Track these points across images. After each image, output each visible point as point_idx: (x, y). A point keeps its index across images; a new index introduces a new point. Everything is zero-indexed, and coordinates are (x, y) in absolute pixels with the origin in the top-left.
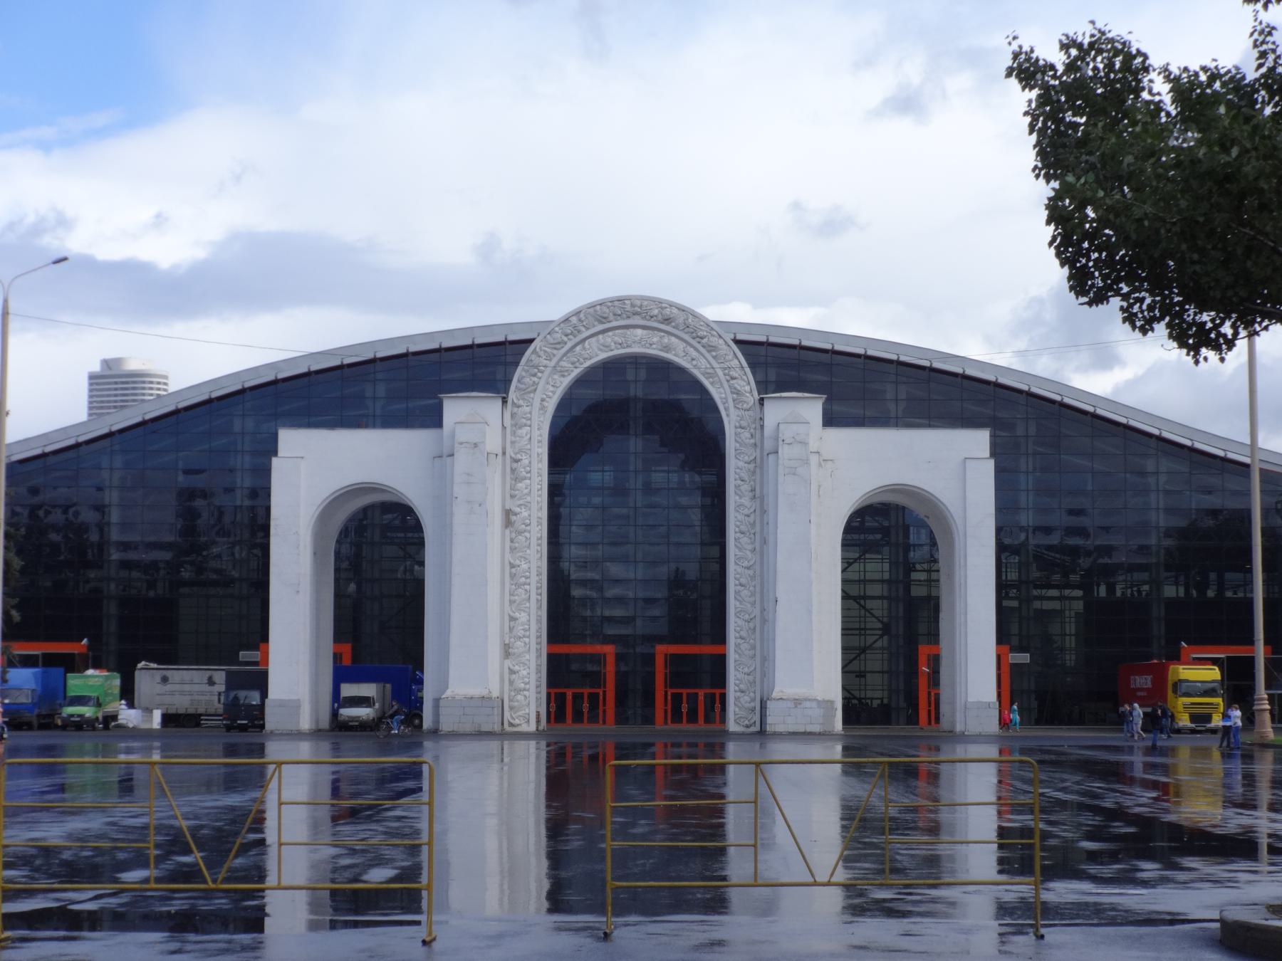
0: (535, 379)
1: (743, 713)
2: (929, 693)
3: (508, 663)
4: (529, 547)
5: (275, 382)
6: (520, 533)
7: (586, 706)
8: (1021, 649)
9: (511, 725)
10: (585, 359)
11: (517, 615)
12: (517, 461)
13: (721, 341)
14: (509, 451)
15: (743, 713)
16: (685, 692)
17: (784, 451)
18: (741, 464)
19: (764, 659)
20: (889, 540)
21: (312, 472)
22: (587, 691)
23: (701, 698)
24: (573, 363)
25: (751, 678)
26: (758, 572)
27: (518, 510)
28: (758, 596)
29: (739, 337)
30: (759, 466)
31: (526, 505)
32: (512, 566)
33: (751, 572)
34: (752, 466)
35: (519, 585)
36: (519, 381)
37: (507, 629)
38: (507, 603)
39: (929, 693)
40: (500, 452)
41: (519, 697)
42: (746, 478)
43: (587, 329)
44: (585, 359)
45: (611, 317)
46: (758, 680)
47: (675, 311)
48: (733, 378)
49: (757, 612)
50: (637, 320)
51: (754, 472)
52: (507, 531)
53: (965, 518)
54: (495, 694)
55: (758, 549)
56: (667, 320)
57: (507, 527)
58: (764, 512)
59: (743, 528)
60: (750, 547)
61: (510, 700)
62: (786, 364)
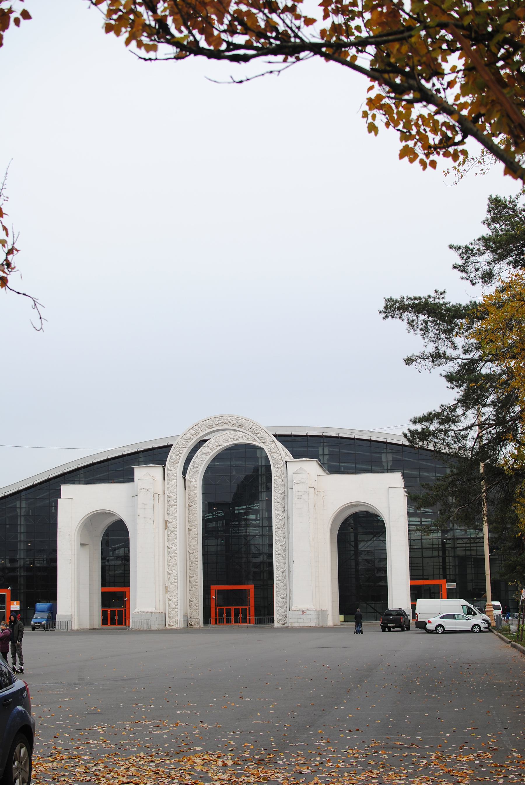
0: (178, 457)
1: (281, 617)
2: (216, 608)
3: (167, 595)
4: (176, 538)
5: (93, 464)
6: (172, 532)
7: (117, 617)
8: (453, 581)
9: (169, 625)
10: (216, 446)
11: (171, 572)
12: (170, 497)
13: (267, 435)
14: (167, 492)
15: (281, 617)
16: (240, 608)
17: (296, 488)
18: (277, 495)
19: (290, 591)
20: (359, 531)
21: (76, 506)
22: (116, 609)
23: (233, 611)
24: (211, 449)
25: (284, 600)
26: (287, 547)
27: (170, 521)
28: (287, 559)
29: (278, 433)
30: (285, 496)
31: (175, 518)
32: (169, 548)
33: (283, 548)
34: (282, 496)
35: (172, 558)
36: (170, 458)
37: (167, 579)
38: (167, 566)
39: (216, 608)
40: (161, 493)
41: (173, 612)
42: (280, 502)
43: (203, 431)
44: (216, 446)
45: (214, 425)
46: (288, 601)
47: (244, 421)
48: (273, 453)
49: (287, 567)
50: (226, 426)
51: (284, 498)
52: (166, 531)
53: (389, 517)
54: (162, 610)
55: (286, 536)
56: (240, 426)
57: (166, 529)
58: (288, 518)
59: (279, 526)
60: (282, 535)
61: (169, 614)
62: (301, 445)
